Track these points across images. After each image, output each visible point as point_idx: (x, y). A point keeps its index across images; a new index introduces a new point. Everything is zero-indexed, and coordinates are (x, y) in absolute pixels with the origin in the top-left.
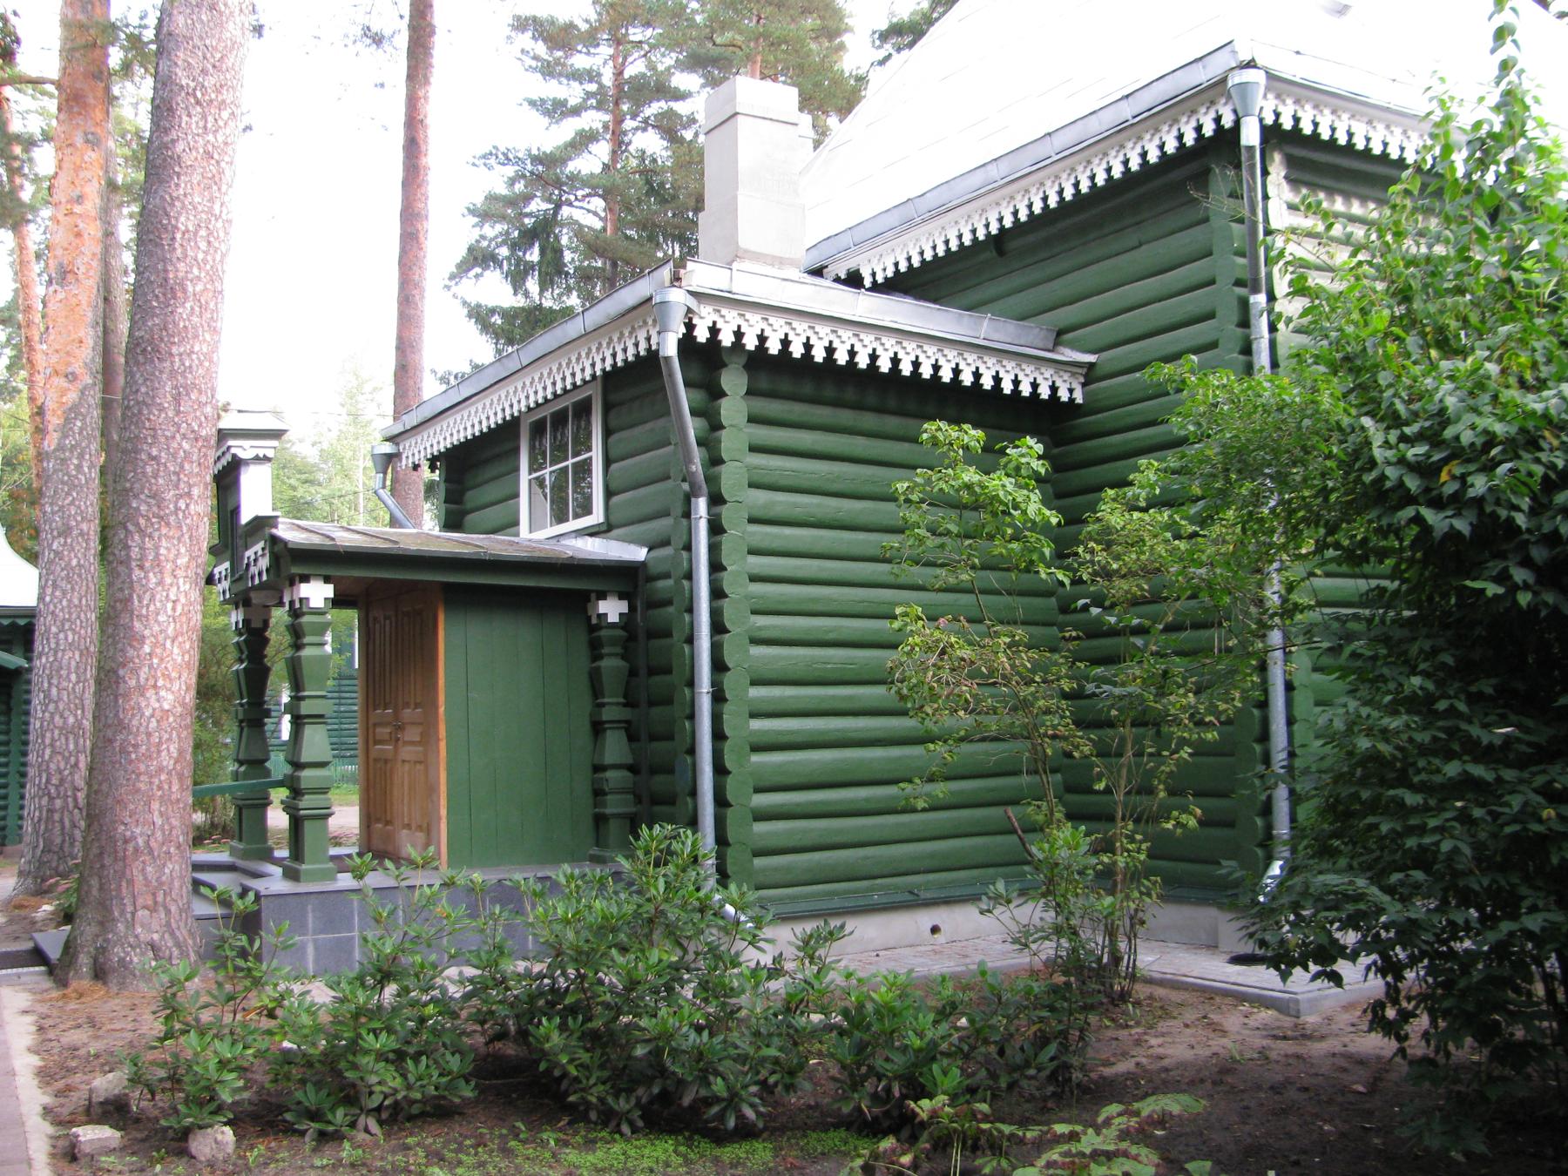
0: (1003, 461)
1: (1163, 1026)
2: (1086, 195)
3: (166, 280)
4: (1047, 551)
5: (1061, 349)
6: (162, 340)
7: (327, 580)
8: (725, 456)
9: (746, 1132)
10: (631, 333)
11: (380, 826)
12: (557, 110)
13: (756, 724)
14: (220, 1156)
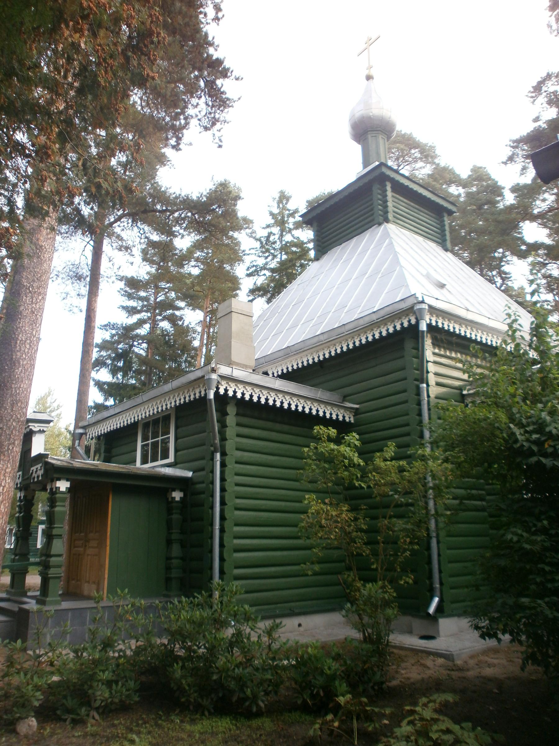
0: (343, 441)
1: (403, 665)
2: (357, 347)
3: (12, 358)
4: (359, 475)
5: (345, 403)
6: (8, 382)
7: (67, 480)
8: (227, 437)
9: (259, 714)
10: (193, 390)
11: (74, 582)
12: (132, 311)
13: (236, 541)
14: (30, 733)
